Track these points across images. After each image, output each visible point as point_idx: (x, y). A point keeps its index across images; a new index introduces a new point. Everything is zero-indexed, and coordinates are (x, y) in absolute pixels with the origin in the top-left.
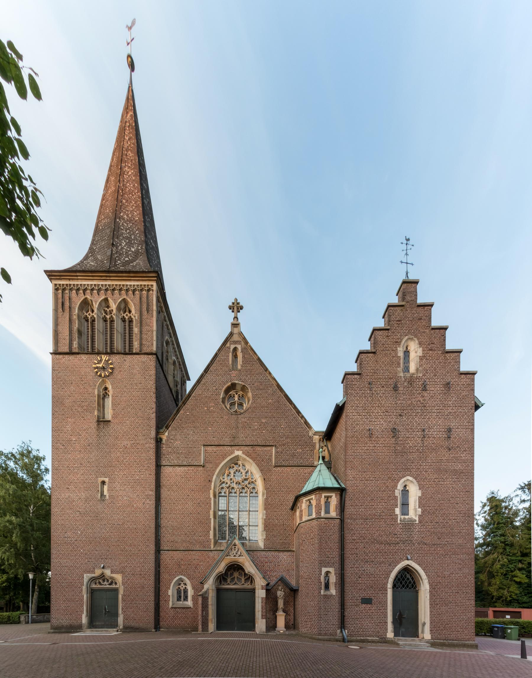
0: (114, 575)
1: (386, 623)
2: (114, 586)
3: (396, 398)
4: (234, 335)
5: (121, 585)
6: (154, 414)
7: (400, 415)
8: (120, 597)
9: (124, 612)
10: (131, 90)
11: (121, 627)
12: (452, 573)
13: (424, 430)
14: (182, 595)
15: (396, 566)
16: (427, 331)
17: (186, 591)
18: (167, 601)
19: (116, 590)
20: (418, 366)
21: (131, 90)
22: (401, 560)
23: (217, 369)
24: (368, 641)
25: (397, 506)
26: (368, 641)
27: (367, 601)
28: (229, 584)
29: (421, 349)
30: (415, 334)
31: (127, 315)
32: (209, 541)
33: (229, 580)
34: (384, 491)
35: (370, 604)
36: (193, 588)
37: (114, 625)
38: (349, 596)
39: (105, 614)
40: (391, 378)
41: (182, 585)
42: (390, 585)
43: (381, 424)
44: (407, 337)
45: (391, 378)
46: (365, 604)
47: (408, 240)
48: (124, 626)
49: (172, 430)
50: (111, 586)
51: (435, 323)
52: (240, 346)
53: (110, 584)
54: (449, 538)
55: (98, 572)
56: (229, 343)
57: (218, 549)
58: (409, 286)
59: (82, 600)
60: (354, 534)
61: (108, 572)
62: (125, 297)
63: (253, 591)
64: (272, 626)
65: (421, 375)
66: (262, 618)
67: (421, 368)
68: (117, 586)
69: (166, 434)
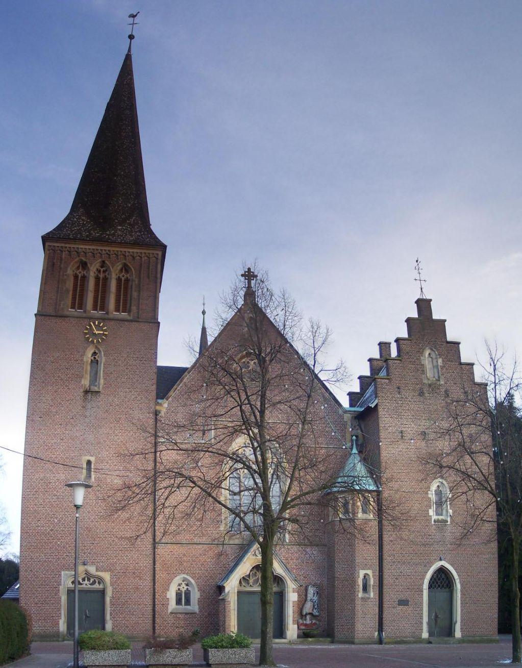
1: (422, 623)
2: (96, 586)
6: (155, 386)
8: (108, 599)
9: (113, 618)
10: (128, 58)
15: (431, 566)
17: (188, 594)
18: (165, 605)
19: (103, 592)
21: (128, 58)
27: (403, 603)
38: (386, 598)
46: (401, 605)
58: (424, 305)
61: (92, 570)
62: (124, 261)
66: (294, 624)
68: (101, 586)
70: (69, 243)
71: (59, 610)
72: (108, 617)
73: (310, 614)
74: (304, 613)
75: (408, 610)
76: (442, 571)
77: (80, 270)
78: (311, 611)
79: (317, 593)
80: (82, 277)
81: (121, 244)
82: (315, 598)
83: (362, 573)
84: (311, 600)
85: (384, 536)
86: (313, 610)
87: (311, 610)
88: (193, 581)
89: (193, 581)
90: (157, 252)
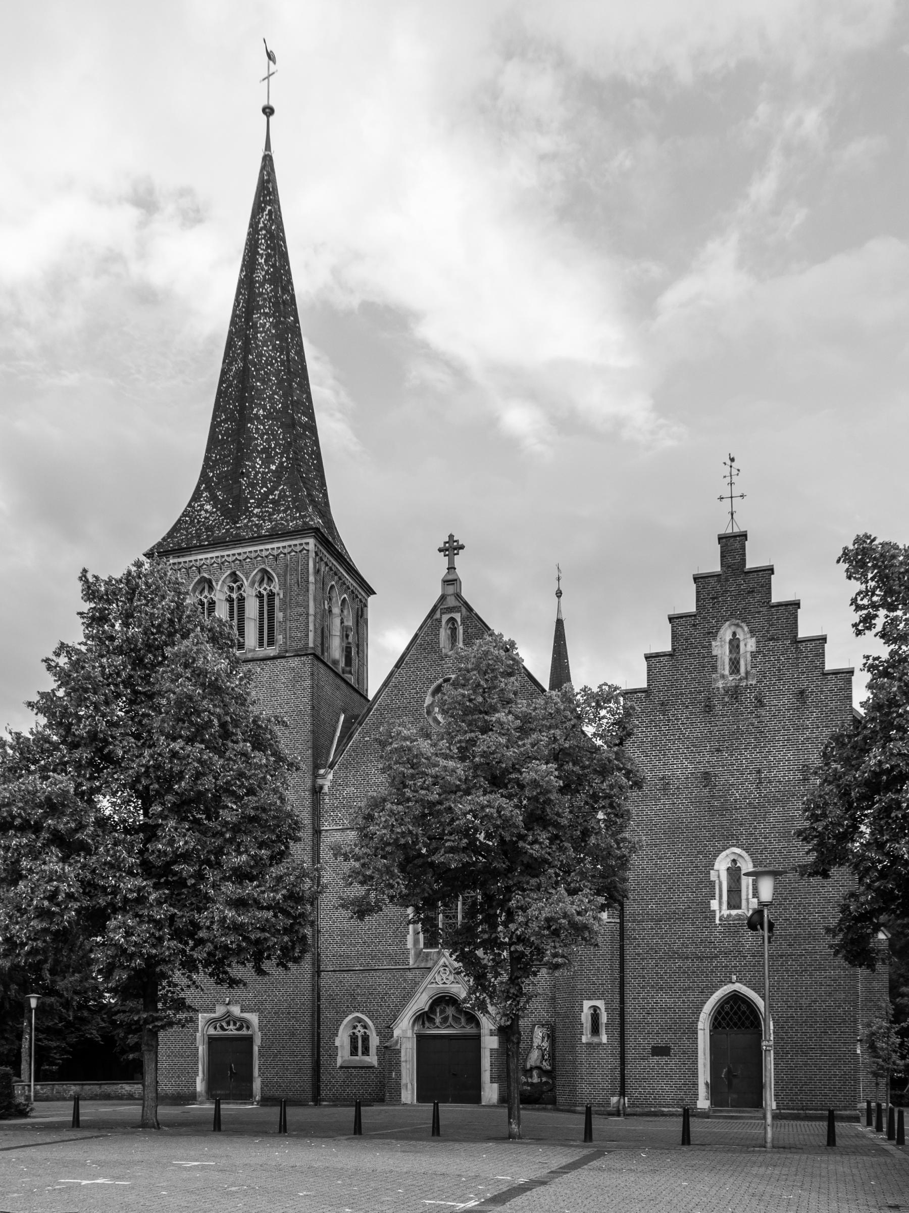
0: (246, 1015)
1: (696, 1084)
2: (244, 1032)
3: (710, 722)
4: (449, 598)
5: (257, 1030)
7: (718, 750)
8: (256, 1049)
10: (268, 161)
11: (258, 1098)
12: (815, 1001)
13: (759, 772)
14: (359, 1044)
16: (764, 609)
17: (366, 1039)
19: (249, 1040)
20: (749, 668)
21: (268, 161)
22: (722, 983)
23: (417, 659)
24: (663, 1114)
25: (713, 897)
27: (661, 1051)
28: (438, 1027)
29: (754, 640)
30: (741, 616)
31: (265, 589)
32: (406, 952)
33: (438, 1021)
34: (691, 873)
35: (666, 1055)
36: (379, 1033)
37: (248, 1096)
38: (630, 1044)
39: (231, 1077)
40: (700, 692)
41: (359, 1028)
42: (704, 1024)
43: (682, 768)
44: (728, 623)
45: (700, 692)
46: (657, 1055)
47: (732, 460)
48: (262, 1097)
49: (340, 769)
50: (240, 1032)
52: (459, 614)
53: (237, 1030)
54: (809, 943)
55: (220, 1010)
56: (438, 612)
57: (423, 965)
58: (732, 545)
59: (196, 1055)
60: (639, 945)
61: (236, 1010)
63: (477, 1038)
64: (130, 1097)
65: (754, 682)
67: (753, 671)
68: (250, 1033)
69: (330, 777)
70: (183, 556)
71: (196, 1063)
72: (256, 1072)
74: (528, 1067)
76: (735, 998)
78: (538, 1064)
79: (549, 1036)
82: (545, 1044)
83: (587, 1004)
85: (627, 947)
86: (541, 1062)
87: (539, 1061)
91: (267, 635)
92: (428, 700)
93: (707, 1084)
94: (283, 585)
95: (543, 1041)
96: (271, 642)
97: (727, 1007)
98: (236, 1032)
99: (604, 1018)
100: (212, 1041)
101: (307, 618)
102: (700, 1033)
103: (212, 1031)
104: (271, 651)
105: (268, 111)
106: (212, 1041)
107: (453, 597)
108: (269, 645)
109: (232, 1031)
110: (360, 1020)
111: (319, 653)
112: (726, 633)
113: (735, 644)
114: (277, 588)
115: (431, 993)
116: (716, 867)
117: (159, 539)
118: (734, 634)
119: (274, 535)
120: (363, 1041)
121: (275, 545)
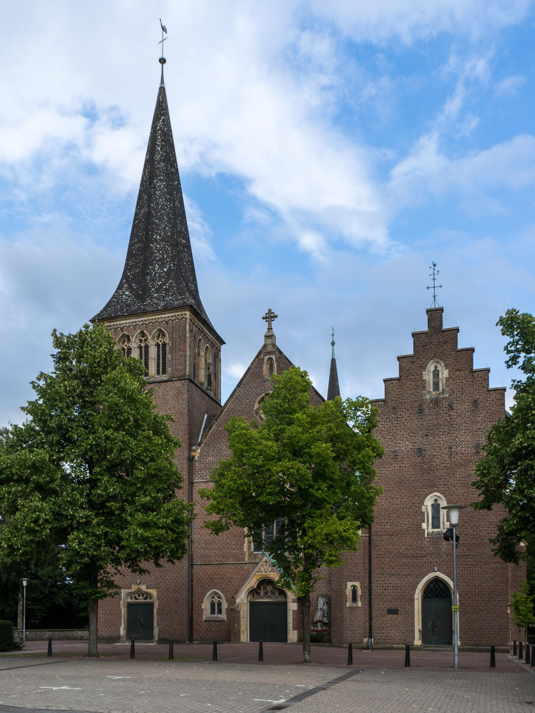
0: (150, 591)
1: (413, 631)
2: (148, 600)
3: (422, 419)
4: (268, 346)
5: (156, 599)
7: (426, 435)
8: (155, 610)
10: (162, 91)
11: (156, 639)
12: (484, 582)
13: (450, 448)
14: (215, 608)
15: (423, 578)
16: (454, 353)
17: (220, 604)
18: (201, 614)
19: (151, 605)
20: (444, 387)
21: (162, 91)
22: (429, 572)
24: (394, 649)
25: (424, 521)
26: (394, 649)
27: (393, 611)
28: (262, 598)
29: (447, 370)
31: (161, 341)
34: (411, 507)
35: (396, 614)
37: (150, 638)
39: (141, 627)
40: (416, 401)
41: (216, 598)
42: (418, 595)
45: (416, 401)
46: (391, 614)
47: (435, 265)
48: (159, 639)
49: (204, 446)
50: (146, 601)
51: (461, 346)
52: (275, 356)
55: (134, 588)
56: (262, 355)
57: (253, 561)
58: (435, 315)
60: (380, 550)
61: (143, 588)
63: (285, 604)
64: (82, 639)
65: (447, 396)
66: (294, 630)
67: (447, 389)
68: (152, 601)
69: (199, 451)
70: (112, 322)
71: (120, 619)
72: (155, 624)
73: (320, 621)
74: (315, 621)
75: (399, 618)
76: (437, 581)
77: (126, 343)
79: (327, 603)
80: (163, 345)
81: (157, 312)
82: (325, 608)
83: (349, 584)
84: (321, 609)
87: (321, 617)
88: (222, 595)
89: (222, 595)
90: (185, 312)
91: (162, 368)
92: (256, 406)
93: (420, 631)
94: (171, 338)
95: (323, 606)
96: (164, 372)
97: (432, 586)
98: (143, 600)
99: (359, 592)
100: (130, 606)
101: (185, 358)
102: (416, 601)
103: (129, 600)
104: (164, 377)
105: (163, 61)
106: (130, 606)
107: (271, 346)
108: (163, 374)
109: (141, 599)
110: (216, 593)
111: (192, 378)
112: (431, 367)
113: (436, 373)
114: (168, 340)
115: (258, 577)
116: (425, 504)
117: (98, 312)
118: (436, 367)
119: (166, 309)
120: (218, 606)
121: (167, 315)
